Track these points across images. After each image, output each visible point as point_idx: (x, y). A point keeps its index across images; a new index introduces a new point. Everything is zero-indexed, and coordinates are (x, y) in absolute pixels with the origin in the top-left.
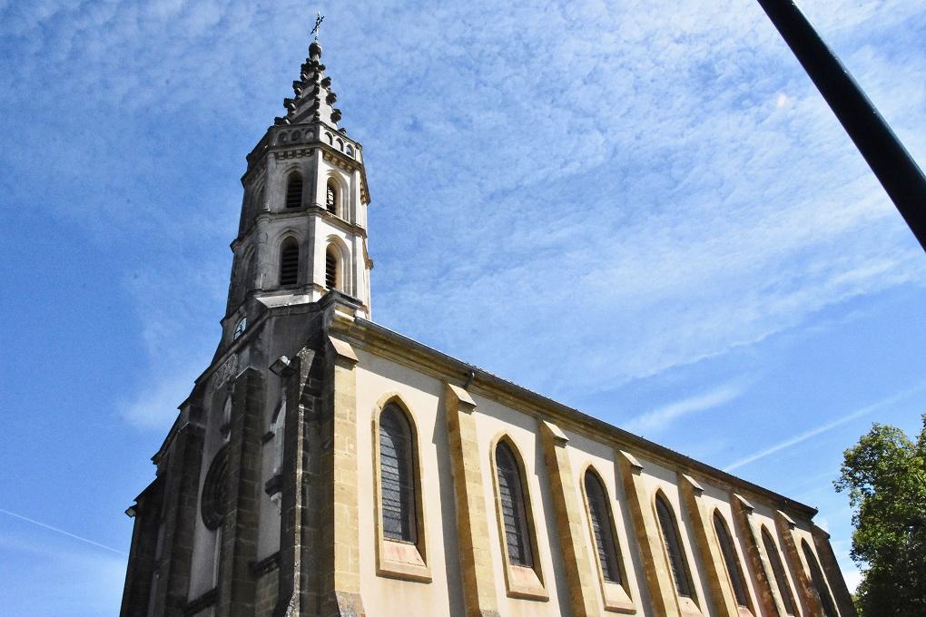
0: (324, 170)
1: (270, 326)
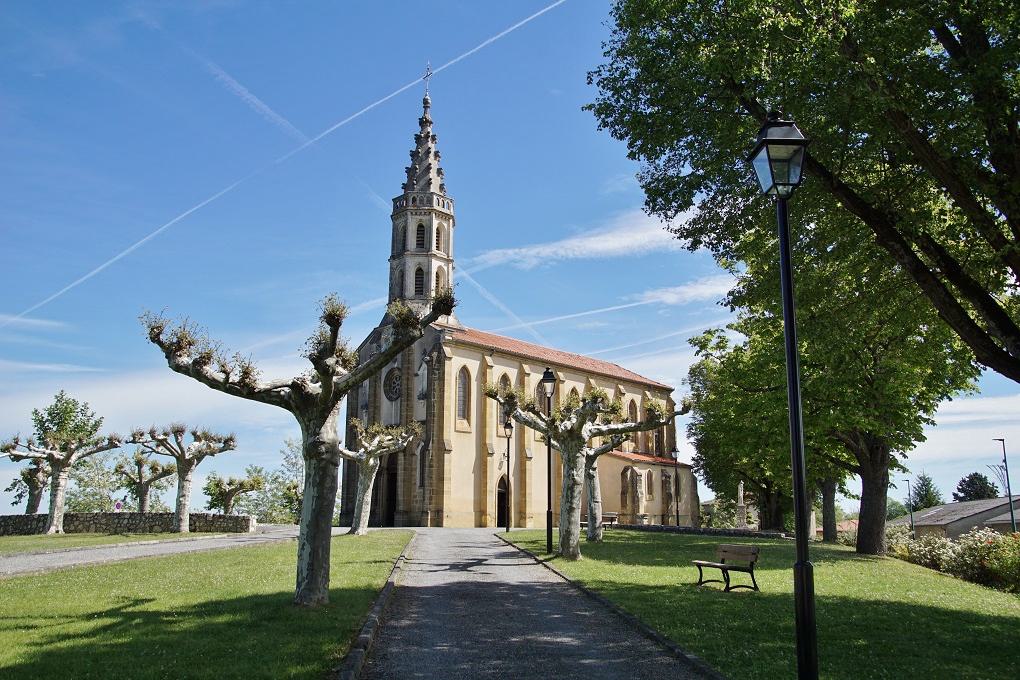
0: (435, 223)
1: (973, 506)
